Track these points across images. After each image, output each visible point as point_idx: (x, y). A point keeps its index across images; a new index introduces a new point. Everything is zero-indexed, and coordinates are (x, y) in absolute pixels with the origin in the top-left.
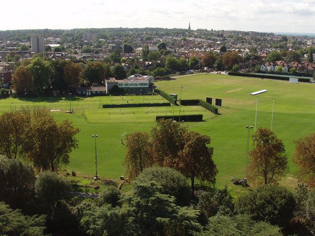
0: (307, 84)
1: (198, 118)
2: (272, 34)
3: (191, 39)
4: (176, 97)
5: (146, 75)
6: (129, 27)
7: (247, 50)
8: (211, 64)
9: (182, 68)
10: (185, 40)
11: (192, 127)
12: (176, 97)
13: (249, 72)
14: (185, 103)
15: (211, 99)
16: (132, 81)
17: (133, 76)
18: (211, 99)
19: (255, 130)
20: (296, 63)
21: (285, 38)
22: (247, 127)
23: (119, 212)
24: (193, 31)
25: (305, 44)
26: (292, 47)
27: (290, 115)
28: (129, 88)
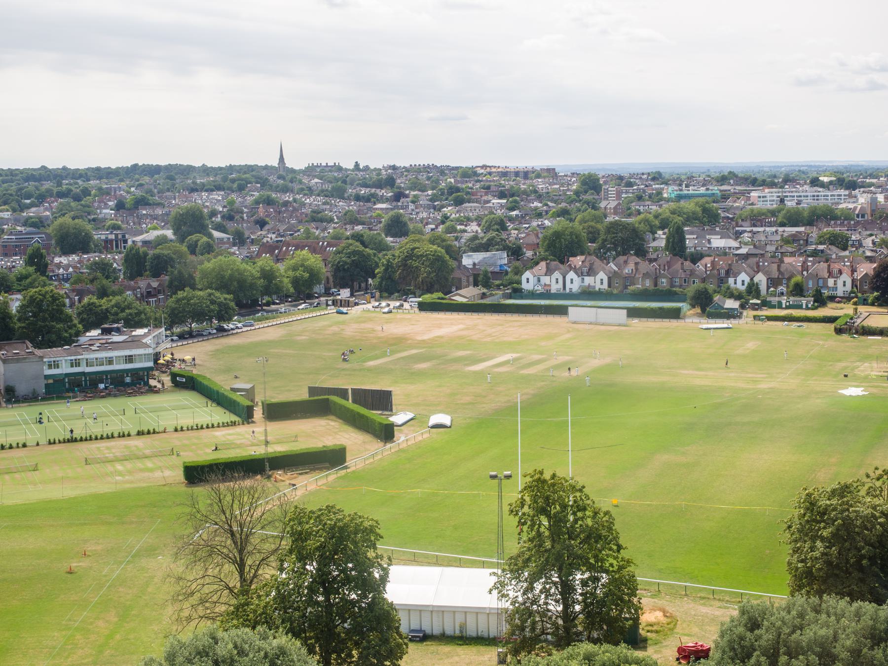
0: (674, 323)
1: (334, 458)
2: (551, 172)
3: (288, 197)
4: (250, 393)
5: (142, 326)
6: (72, 166)
7: (474, 227)
8: (357, 274)
9: (251, 298)
10: (269, 202)
11: (305, 490)
12: (250, 393)
13: (484, 296)
14: (277, 412)
15: (389, 393)
16: (96, 352)
17: (95, 333)
18: (389, 393)
19: (520, 482)
20: (633, 260)
21: (591, 183)
22: (493, 477)
23: (637, 264)
24: (293, 171)
25: (657, 197)
26: (616, 211)
27: (81, 176)
28: (83, 374)
